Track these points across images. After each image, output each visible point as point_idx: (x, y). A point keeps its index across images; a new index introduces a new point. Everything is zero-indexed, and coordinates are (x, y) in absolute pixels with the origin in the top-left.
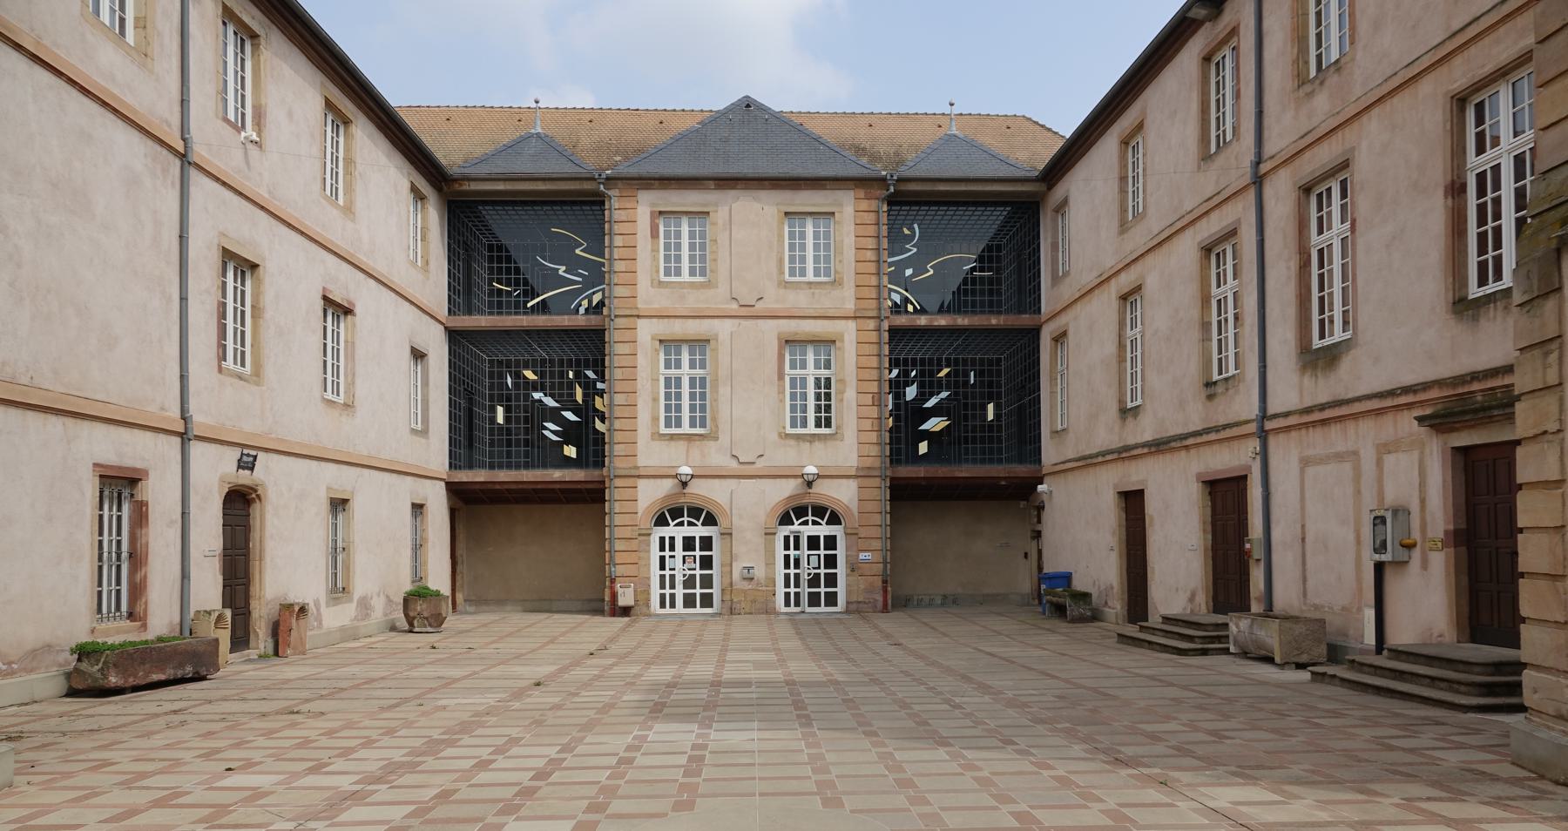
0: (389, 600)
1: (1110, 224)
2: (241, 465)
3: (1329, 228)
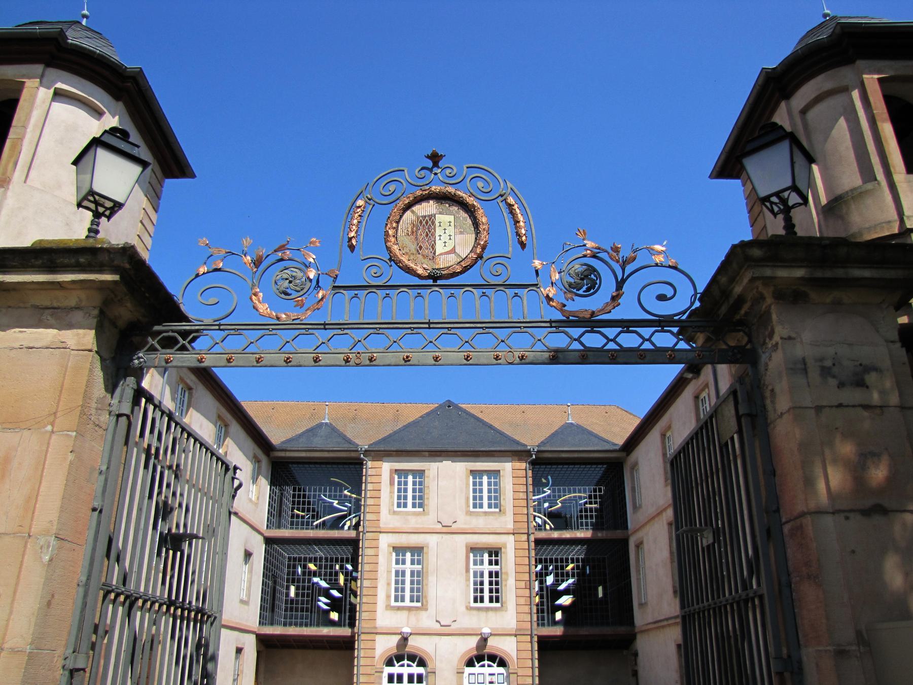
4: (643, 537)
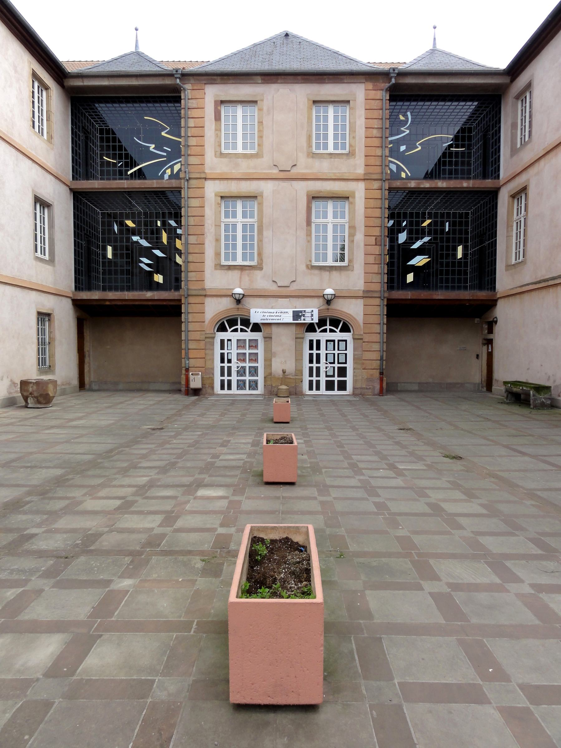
0: (13, 383)
4: (528, 180)
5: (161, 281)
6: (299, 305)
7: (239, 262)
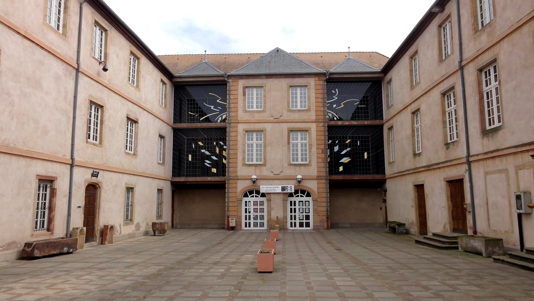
0: (148, 224)
1: (407, 87)
2: (93, 175)
3: (490, 84)
5: (215, 172)
6: (285, 184)
7: (255, 162)
